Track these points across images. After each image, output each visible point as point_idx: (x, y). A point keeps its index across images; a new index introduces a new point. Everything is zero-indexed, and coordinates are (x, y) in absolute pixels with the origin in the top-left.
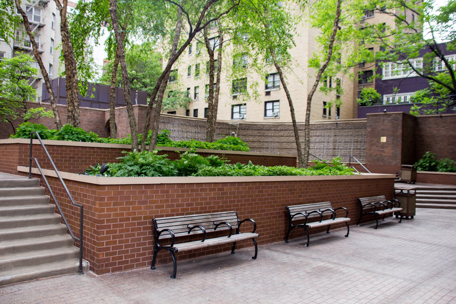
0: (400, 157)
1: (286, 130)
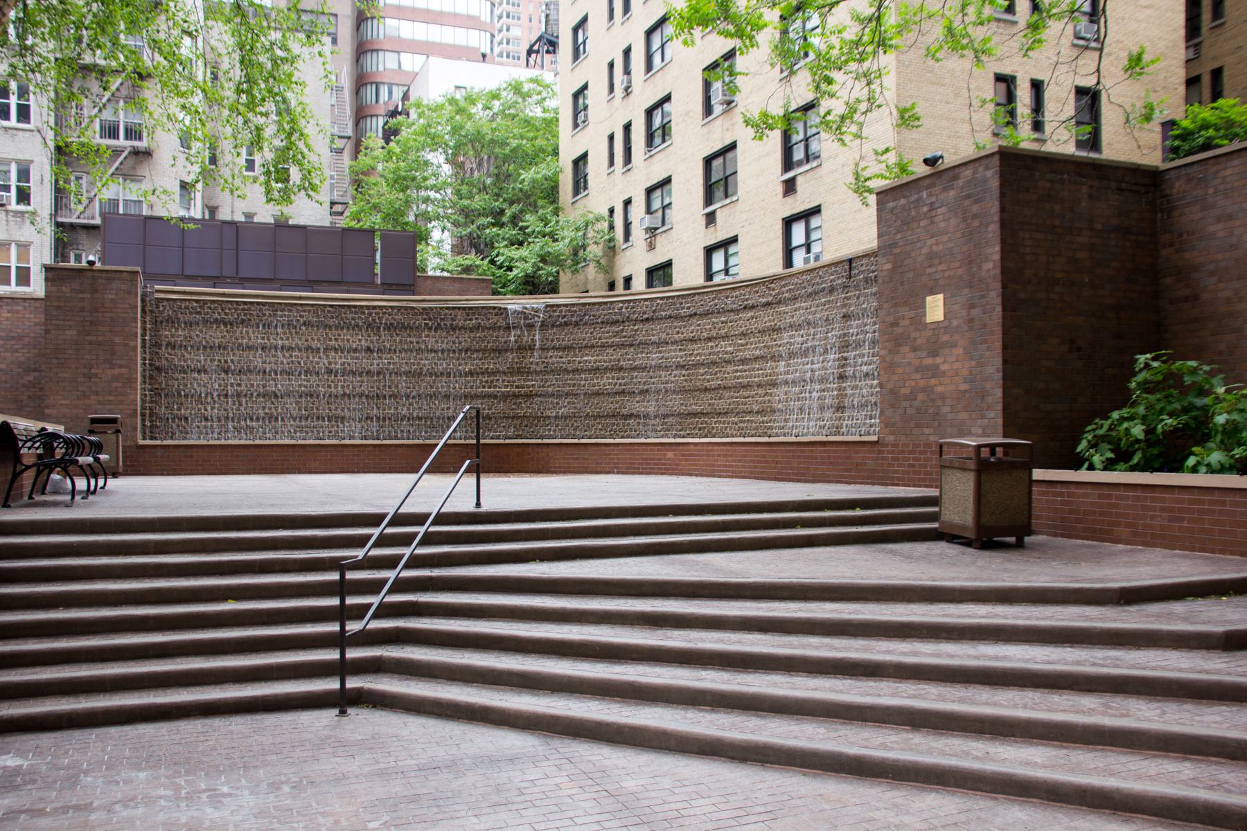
0: (999, 393)
1: (707, 314)
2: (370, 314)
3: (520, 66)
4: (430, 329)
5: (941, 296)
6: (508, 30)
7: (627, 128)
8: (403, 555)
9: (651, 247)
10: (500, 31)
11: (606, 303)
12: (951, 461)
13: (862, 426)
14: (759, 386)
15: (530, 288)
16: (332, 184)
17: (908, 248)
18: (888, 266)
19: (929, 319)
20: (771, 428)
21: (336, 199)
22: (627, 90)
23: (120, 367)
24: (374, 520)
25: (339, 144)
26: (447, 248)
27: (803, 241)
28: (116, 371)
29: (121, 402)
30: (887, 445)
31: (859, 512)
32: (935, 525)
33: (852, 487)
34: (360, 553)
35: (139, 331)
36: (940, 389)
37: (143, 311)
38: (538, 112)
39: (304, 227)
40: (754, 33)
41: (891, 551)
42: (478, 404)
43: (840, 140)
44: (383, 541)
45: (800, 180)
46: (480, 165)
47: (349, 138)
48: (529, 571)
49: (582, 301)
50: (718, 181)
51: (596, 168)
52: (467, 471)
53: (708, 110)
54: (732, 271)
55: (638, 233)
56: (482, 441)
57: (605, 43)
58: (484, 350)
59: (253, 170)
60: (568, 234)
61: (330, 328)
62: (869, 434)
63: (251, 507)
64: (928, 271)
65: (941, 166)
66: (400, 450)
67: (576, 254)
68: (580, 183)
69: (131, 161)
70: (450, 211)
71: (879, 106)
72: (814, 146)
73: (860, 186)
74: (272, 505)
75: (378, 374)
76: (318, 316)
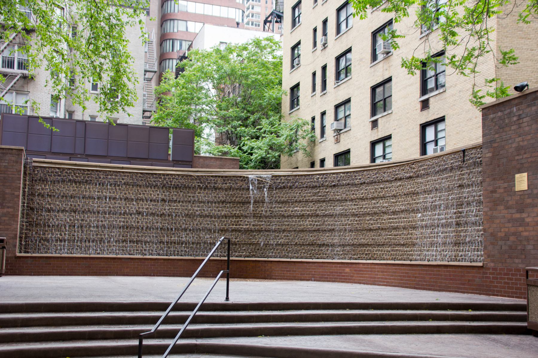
1: (371, 183)
2: (165, 179)
3: (259, 30)
4: (201, 188)
5: (525, 174)
6: (253, 8)
7: (324, 68)
8: (180, 330)
9: (337, 141)
10: (248, 9)
11: (309, 175)
12: (535, 282)
13: (473, 257)
14: (404, 228)
15: (262, 165)
16: (144, 100)
17: (503, 143)
18: (490, 155)
19: (517, 188)
20: (412, 255)
21: (146, 108)
22: (325, 46)
23: (8, 207)
24: (163, 307)
25: (149, 75)
26: (212, 139)
27: (433, 138)
28: (5, 210)
29: (7, 229)
30: (489, 269)
31: (471, 312)
32: (525, 324)
33: (466, 295)
34: (152, 328)
35: (22, 186)
36: (525, 234)
37: (25, 173)
38: (270, 58)
39: (126, 125)
40: (406, 7)
41: (494, 340)
42: (228, 235)
43: (462, 73)
44: (168, 320)
45: (431, 101)
46: (234, 89)
47: (155, 72)
48: (257, 342)
49: (295, 173)
50: (380, 100)
51: (304, 92)
52: (221, 277)
53: (374, 57)
54: (387, 156)
55: (329, 132)
56: (231, 258)
57: (311, 17)
58: (234, 202)
59: (97, 90)
60: (285, 133)
61: (140, 186)
62: (477, 261)
63: (85, 297)
64: (517, 158)
65: (526, 91)
66: (180, 263)
67: (291, 144)
68: (294, 102)
69: (21, 82)
70: (215, 117)
71: (487, 52)
72: (441, 79)
73: (476, 99)
74: (99, 296)
75: (169, 215)
76: (133, 179)
